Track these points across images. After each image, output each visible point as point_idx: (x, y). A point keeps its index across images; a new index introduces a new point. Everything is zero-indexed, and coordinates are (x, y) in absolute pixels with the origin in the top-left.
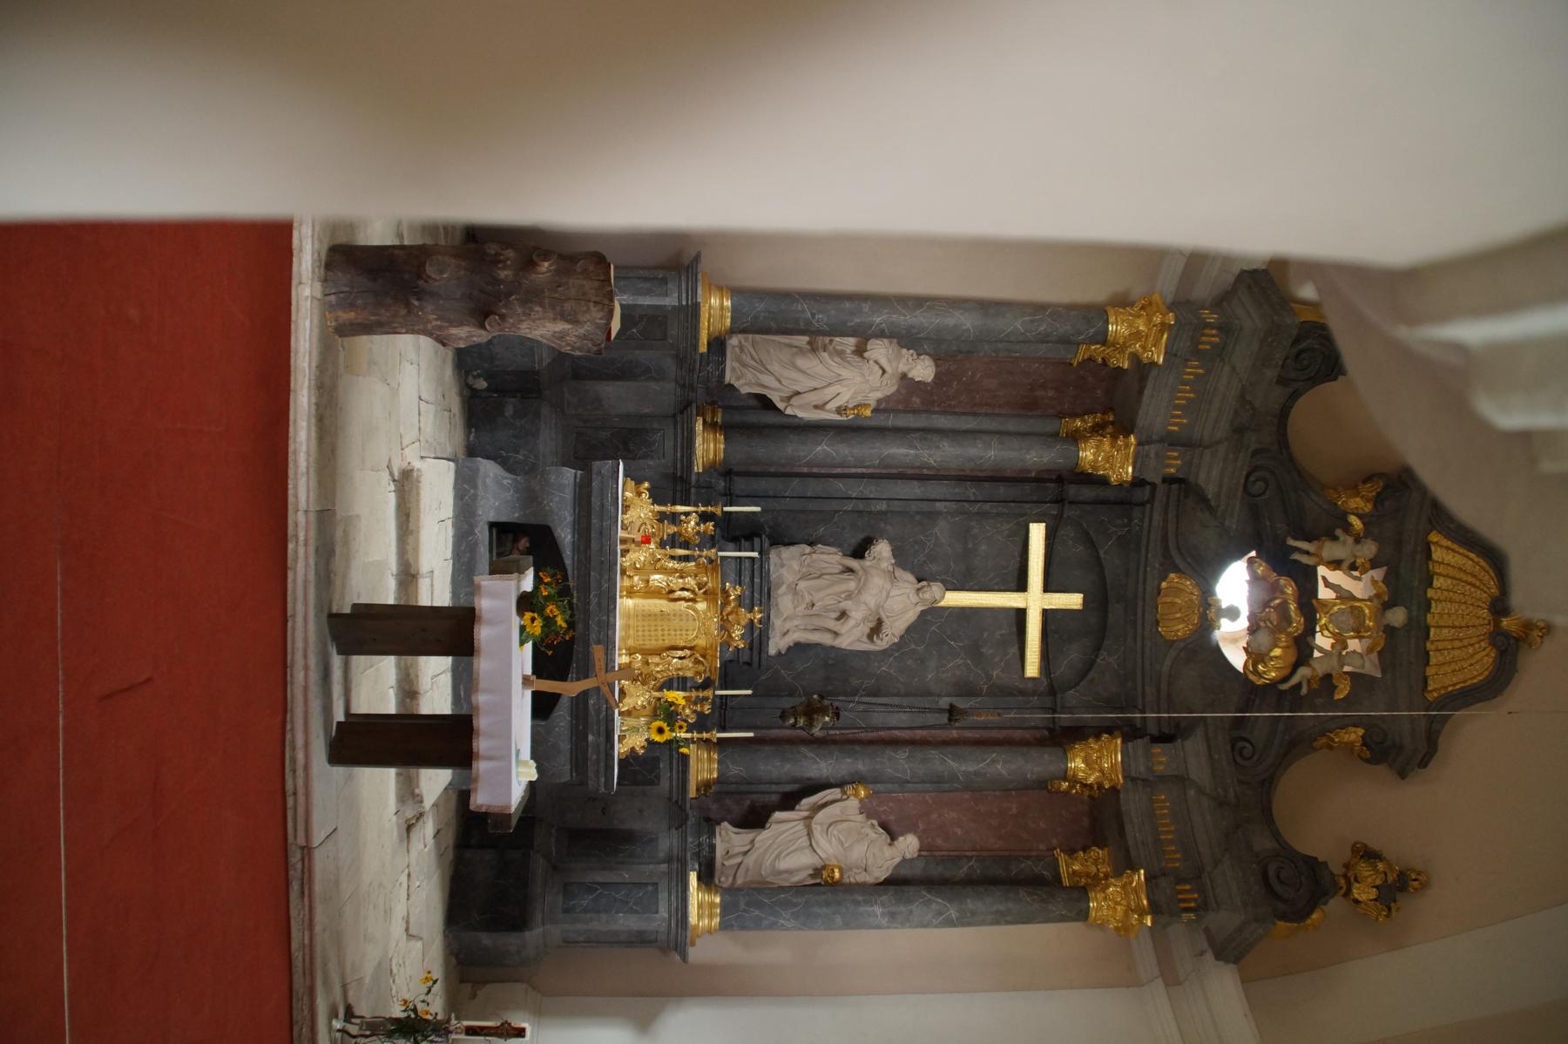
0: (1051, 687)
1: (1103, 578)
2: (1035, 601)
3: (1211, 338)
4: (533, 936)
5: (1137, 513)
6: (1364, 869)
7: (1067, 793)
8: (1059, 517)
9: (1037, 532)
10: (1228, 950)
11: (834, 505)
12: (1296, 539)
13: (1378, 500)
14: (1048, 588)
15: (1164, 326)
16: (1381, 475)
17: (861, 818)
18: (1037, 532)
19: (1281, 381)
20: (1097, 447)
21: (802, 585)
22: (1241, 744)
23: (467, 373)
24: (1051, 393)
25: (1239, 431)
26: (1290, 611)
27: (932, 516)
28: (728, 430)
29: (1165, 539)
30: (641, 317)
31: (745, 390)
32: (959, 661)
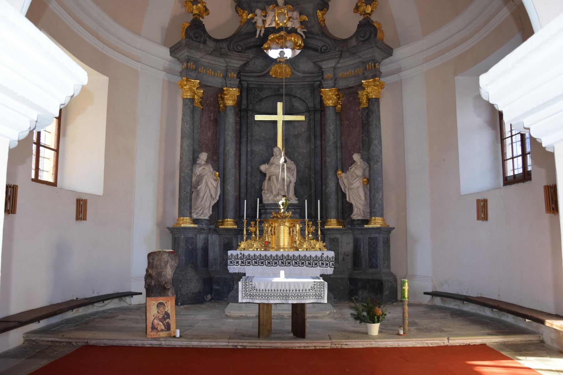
0: (306, 112)
1: (272, 96)
2: (280, 118)
3: (191, 65)
4: (384, 278)
5: (251, 86)
6: (361, 9)
7: (342, 105)
8: (251, 110)
9: (258, 118)
10: (388, 52)
11: (249, 183)
12: (256, 35)
13: (244, 9)
14: (275, 113)
15: (187, 80)
16: (236, 8)
17: (348, 172)
18: (258, 118)
19: (205, 43)
20: (228, 100)
21: (274, 193)
22: (323, 50)
23: (205, 301)
24: (212, 115)
25: (222, 55)
26: (280, 34)
27: (252, 152)
28: (224, 217)
29: (259, 77)
30: (186, 245)
31: (211, 213)
32: (300, 142)
